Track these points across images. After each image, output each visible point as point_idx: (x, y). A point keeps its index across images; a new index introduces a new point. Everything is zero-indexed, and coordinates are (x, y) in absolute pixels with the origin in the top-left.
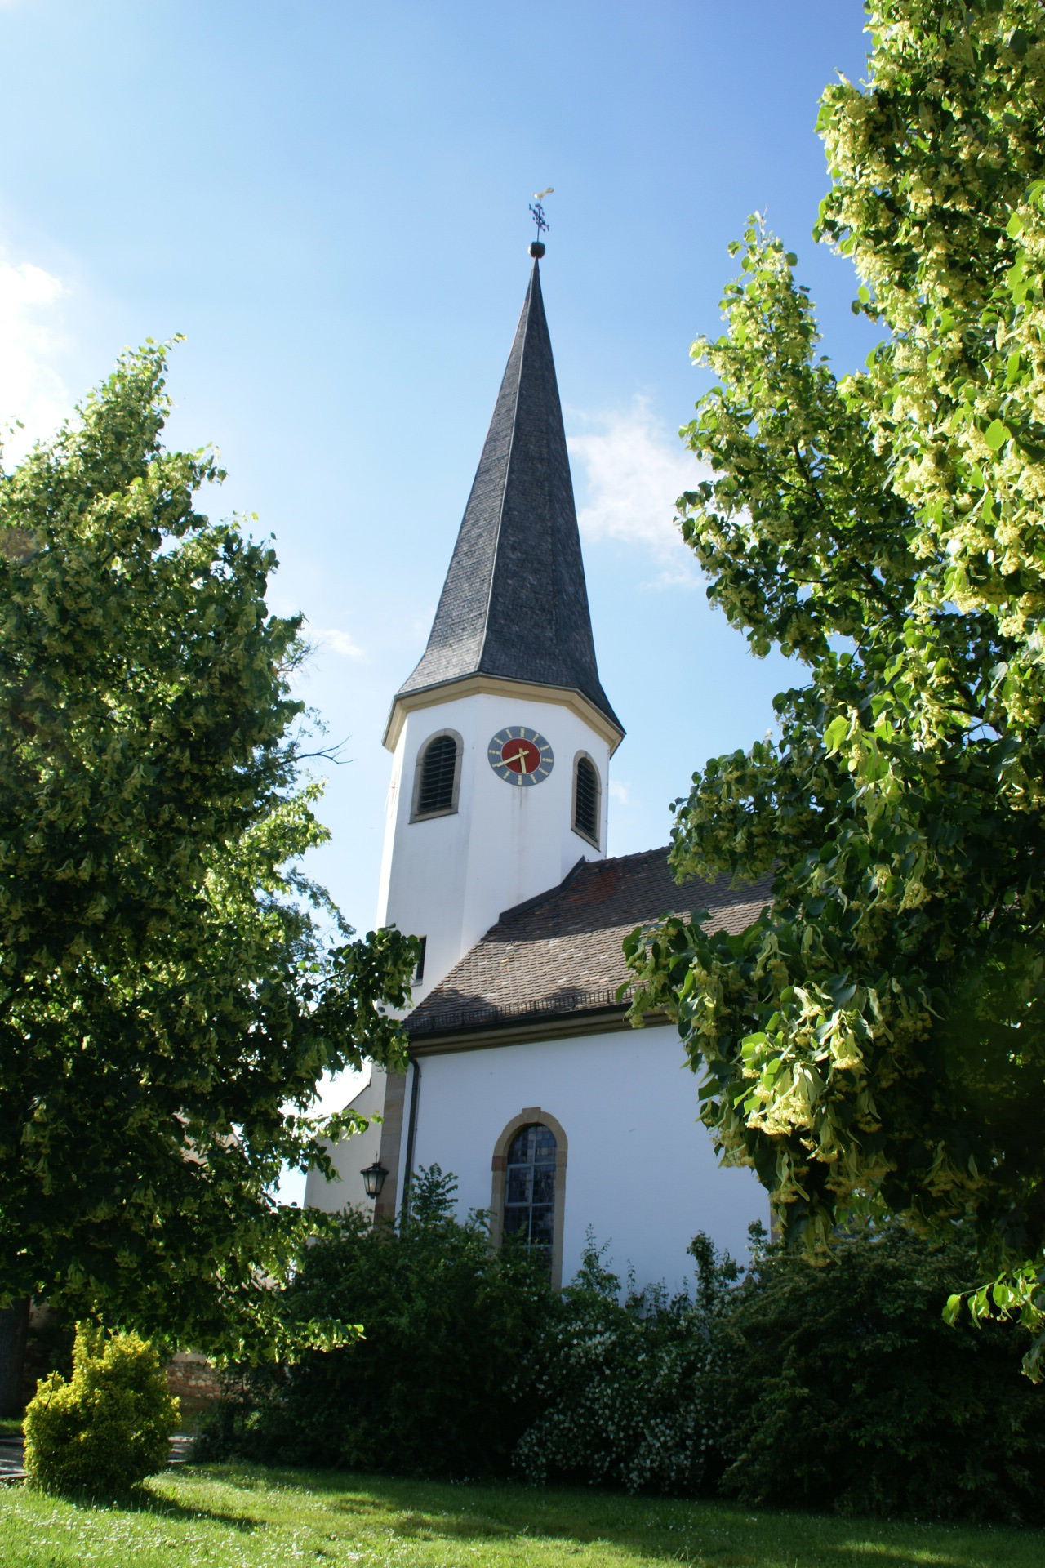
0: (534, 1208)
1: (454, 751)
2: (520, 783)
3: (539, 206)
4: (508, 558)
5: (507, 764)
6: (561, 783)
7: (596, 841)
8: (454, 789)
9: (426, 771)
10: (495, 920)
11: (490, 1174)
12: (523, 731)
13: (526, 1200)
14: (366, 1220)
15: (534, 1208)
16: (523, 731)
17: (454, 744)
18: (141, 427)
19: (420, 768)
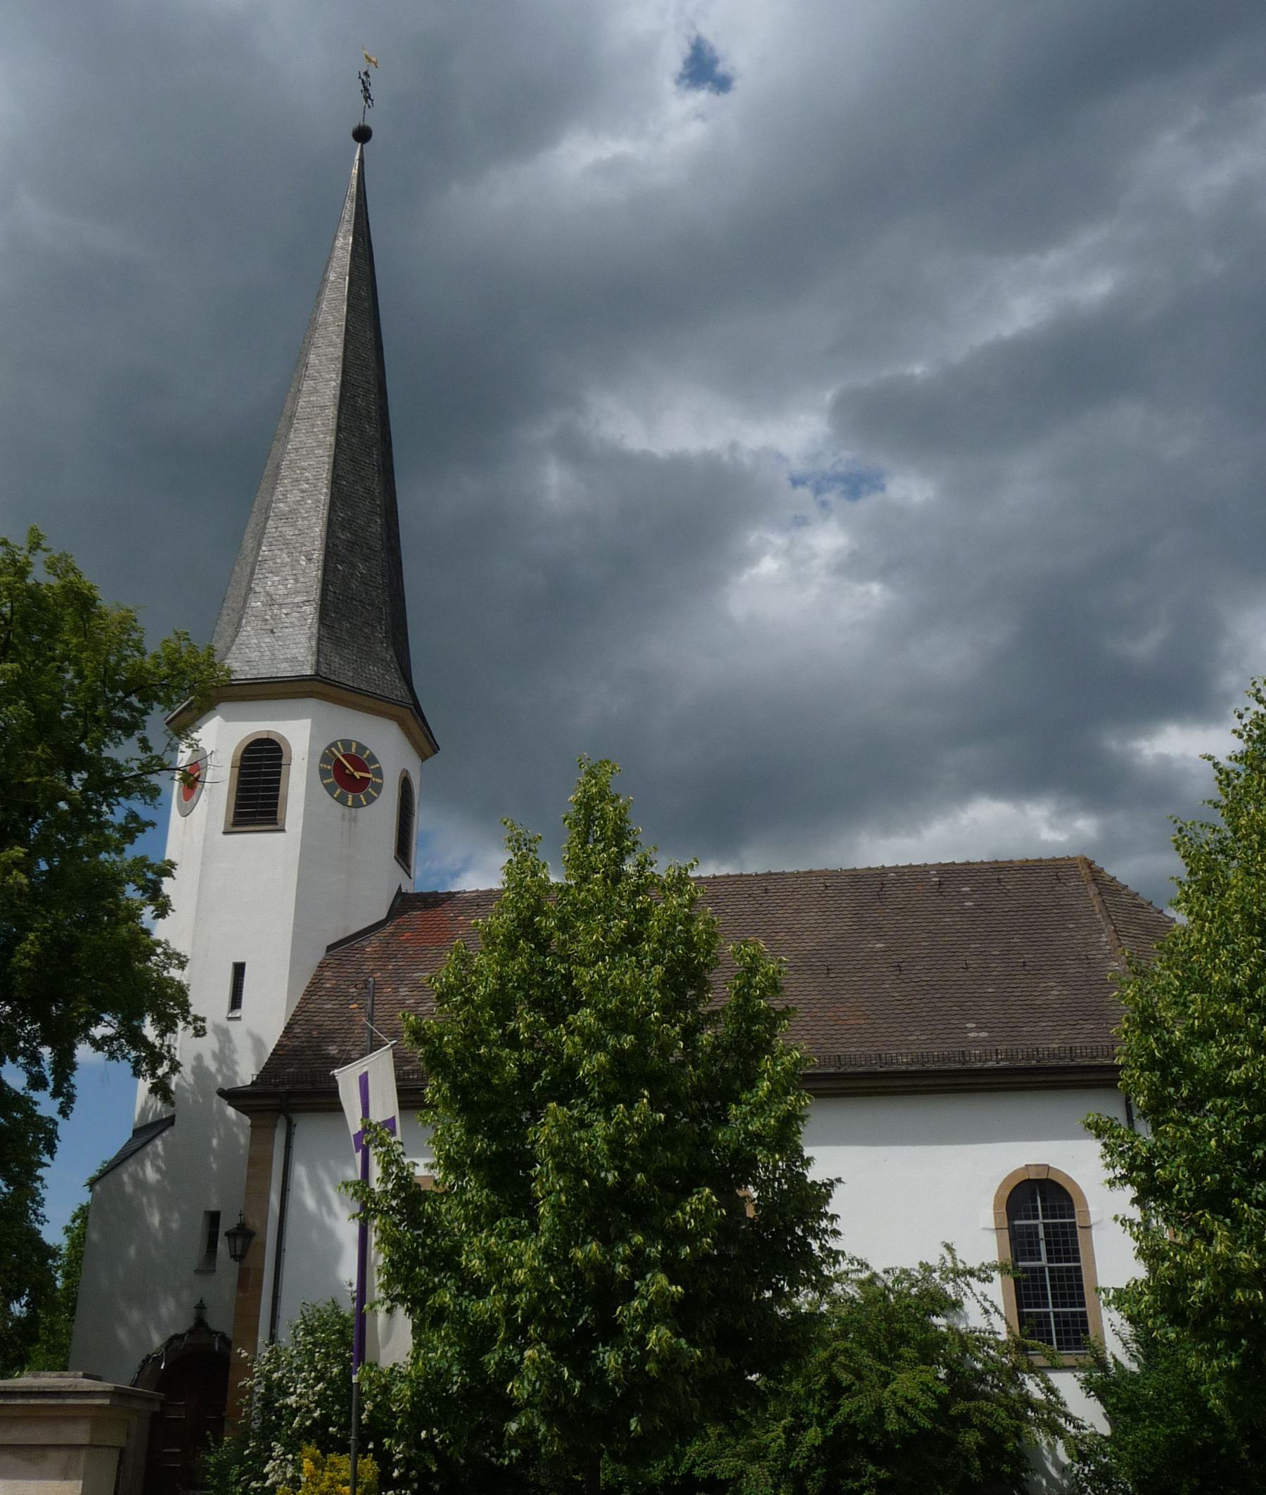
0: (1044, 1217)
1: (280, 758)
2: (350, 803)
3: (366, 74)
4: (338, 538)
5: (338, 759)
6: (387, 804)
7: (409, 867)
8: (280, 801)
9: (241, 774)
10: (321, 954)
11: (204, 727)
12: (354, 745)
13: (1040, 1260)
14: (570, 1018)
15: (1044, 1217)
16: (354, 745)
17: (279, 750)
18: (280, 1417)
19: (237, 770)
